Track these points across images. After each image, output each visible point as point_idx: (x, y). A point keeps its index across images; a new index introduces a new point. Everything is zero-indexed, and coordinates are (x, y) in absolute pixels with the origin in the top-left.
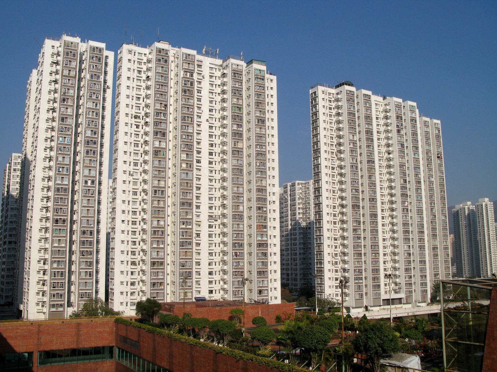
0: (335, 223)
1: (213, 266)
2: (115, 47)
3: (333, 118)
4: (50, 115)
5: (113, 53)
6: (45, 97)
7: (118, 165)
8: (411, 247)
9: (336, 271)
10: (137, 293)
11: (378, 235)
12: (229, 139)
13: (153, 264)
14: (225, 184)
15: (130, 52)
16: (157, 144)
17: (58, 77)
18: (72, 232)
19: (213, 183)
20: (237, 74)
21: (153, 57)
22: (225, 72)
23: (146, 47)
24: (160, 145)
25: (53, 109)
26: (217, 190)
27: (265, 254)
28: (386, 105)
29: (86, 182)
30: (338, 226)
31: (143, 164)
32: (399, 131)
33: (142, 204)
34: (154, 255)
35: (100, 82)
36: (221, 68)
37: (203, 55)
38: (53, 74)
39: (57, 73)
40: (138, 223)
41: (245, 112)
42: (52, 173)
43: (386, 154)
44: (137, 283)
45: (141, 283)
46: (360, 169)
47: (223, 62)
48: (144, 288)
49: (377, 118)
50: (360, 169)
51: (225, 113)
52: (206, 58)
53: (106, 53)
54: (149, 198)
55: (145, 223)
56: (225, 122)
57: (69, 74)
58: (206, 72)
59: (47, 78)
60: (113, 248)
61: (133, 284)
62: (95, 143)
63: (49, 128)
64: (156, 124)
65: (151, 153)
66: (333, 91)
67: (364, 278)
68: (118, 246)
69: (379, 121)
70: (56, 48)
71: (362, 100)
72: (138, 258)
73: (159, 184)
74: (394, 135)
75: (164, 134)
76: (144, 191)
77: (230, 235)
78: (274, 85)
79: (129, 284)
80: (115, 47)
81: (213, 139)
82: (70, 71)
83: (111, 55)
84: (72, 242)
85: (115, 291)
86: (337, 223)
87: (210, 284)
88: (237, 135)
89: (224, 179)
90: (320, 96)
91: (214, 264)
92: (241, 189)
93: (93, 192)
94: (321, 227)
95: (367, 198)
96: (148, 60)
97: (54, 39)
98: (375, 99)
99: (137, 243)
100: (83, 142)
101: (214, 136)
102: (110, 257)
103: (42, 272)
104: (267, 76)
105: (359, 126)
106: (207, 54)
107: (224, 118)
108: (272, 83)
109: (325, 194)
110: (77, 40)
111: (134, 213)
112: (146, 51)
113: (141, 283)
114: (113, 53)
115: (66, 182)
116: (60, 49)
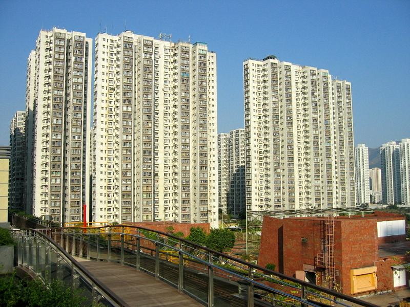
0: (261, 164)
1: (168, 197)
2: (93, 35)
3: (260, 73)
4: (46, 88)
5: (92, 39)
6: (42, 88)
7: (97, 182)
8: (320, 154)
9: (262, 200)
10: (112, 217)
11: (293, 167)
12: (179, 204)
13: (123, 195)
14: (176, 177)
15: (104, 39)
16: (125, 109)
17: (51, 59)
18: (65, 173)
19: (167, 136)
20: (185, 52)
21: (121, 43)
22: (176, 52)
23: (116, 35)
24: (127, 109)
25: (49, 84)
26: (171, 141)
27: (206, 188)
28: (303, 72)
29: (74, 137)
30: (263, 167)
31: (115, 123)
32: (313, 93)
33: (115, 152)
34: (124, 189)
35: (82, 62)
36: (173, 49)
37: (159, 39)
38: (45, 129)
39: (50, 56)
40: (112, 166)
41: (191, 76)
42: (49, 131)
43: (303, 111)
44: (112, 209)
45: (115, 209)
46: (279, 120)
47: (175, 44)
48: (117, 206)
49: (297, 83)
50: (279, 120)
51: (176, 84)
52: (162, 42)
53: (87, 39)
54: (120, 148)
55: (117, 181)
56: (176, 90)
57: (59, 57)
58: (161, 52)
59: (43, 53)
60: (94, 185)
61: (109, 210)
62: (78, 159)
63: (46, 98)
64: (124, 94)
65: (121, 115)
66: (261, 63)
67: (282, 206)
68: (97, 182)
69: (298, 85)
70: (49, 37)
71: (283, 69)
72: (113, 184)
73: (127, 138)
74: (309, 95)
75: (130, 102)
76: (117, 143)
77: (180, 174)
78: (214, 60)
79: (106, 210)
80: (93, 35)
81: (168, 103)
82: (60, 55)
83: (90, 41)
84: (65, 180)
85: (96, 215)
86: (263, 164)
87: (166, 212)
88: (185, 127)
89: (175, 133)
90: (251, 67)
91: (168, 195)
92: (187, 141)
93: (80, 158)
94: (250, 168)
95: (286, 145)
96: (117, 45)
97: (47, 31)
98: (294, 68)
99: (112, 181)
100: (70, 104)
101: (168, 101)
102: (93, 183)
103: (44, 202)
104: (208, 54)
105: (280, 79)
106: (162, 39)
107: (175, 87)
108: (212, 61)
109: (253, 136)
110: (64, 31)
111: (110, 159)
112: (116, 38)
113: (115, 209)
114: (92, 39)
115: (59, 137)
116: (52, 38)
